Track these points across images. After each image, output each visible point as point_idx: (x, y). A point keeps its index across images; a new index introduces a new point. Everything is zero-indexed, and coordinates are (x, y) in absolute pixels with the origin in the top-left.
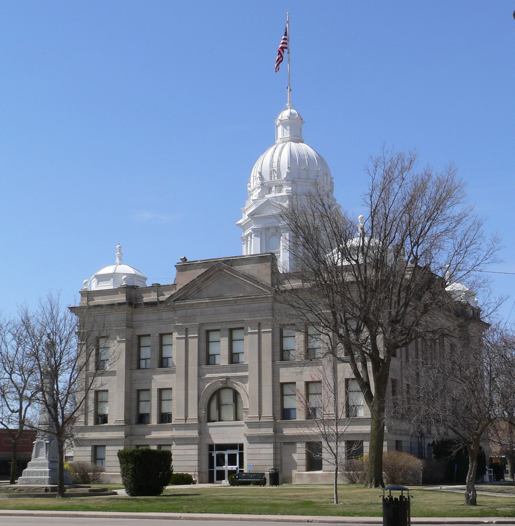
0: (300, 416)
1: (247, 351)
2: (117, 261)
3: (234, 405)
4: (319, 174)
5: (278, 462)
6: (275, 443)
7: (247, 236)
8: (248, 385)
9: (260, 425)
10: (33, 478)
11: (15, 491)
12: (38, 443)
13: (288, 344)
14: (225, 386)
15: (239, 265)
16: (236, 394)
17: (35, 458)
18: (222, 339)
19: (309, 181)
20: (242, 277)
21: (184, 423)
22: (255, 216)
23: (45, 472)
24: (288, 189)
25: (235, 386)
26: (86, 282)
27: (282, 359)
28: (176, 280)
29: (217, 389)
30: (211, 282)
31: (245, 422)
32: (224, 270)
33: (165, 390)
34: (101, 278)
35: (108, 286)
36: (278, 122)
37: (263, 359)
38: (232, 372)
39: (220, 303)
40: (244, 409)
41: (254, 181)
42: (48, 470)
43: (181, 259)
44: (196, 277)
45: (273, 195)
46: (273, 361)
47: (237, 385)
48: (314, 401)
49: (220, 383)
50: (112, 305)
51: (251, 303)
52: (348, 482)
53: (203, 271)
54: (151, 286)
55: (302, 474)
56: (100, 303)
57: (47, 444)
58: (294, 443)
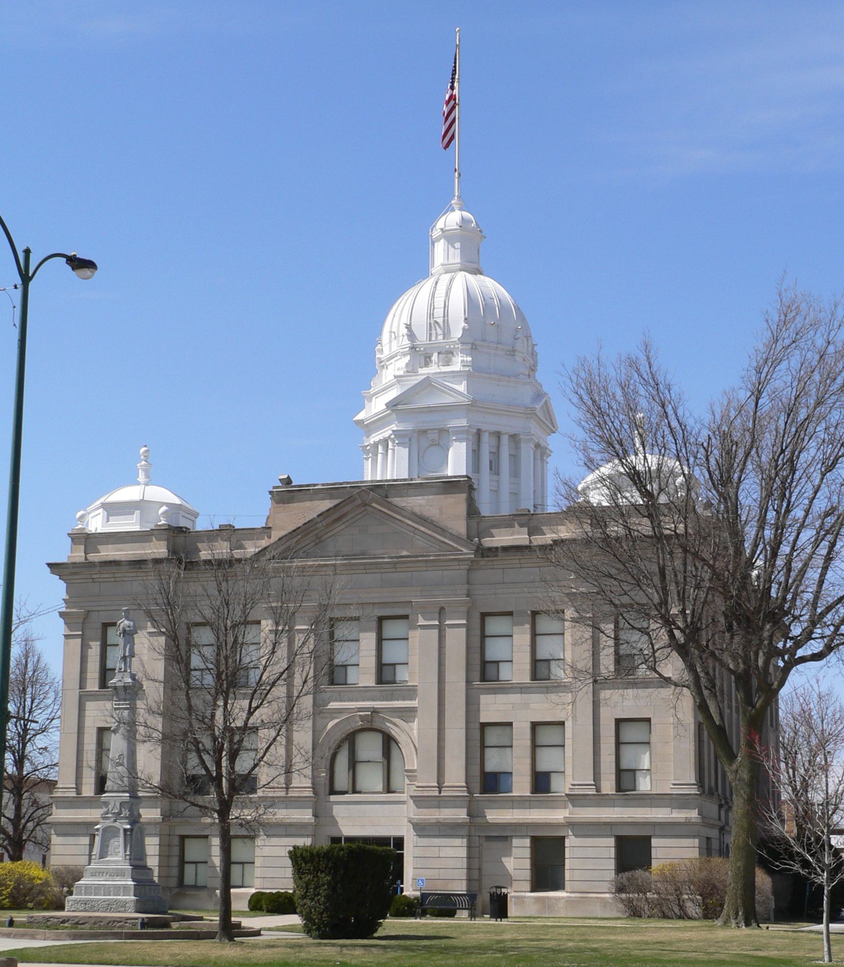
0: (521, 786)
1: (414, 660)
2: (141, 478)
3: (386, 763)
4: (518, 336)
5: (475, 875)
6: (469, 837)
7: (376, 445)
8: (415, 725)
9: (439, 801)
10: (100, 899)
11: (66, 925)
12: (105, 830)
13: (495, 650)
14: (368, 725)
15: (401, 497)
16: (389, 742)
17: (100, 858)
18: (362, 635)
19: (500, 346)
20: (409, 519)
21: (283, 794)
22: (400, 407)
23: (125, 887)
24: (465, 359)
25: (389, 727)
26: (82, 517)
27: (483, 679)
28: (270, 520)
29: (352, 730)
30: (343, 526)
31: (411, 797)
32: (374, 505)
33: (542, 726)
34: (113, 510)
35: (130, 524)
36: (436, 233)
37: (449, 677)
38: (383, 700)
39: (362, 567)
40: (407, 771)
41: (390, 342)
42: (132, 883)
43: (280, 480)
44: (315, 516)
45: (433, 369)
46: (468, 682)
47: (395, 724)
48: (547, 761)
49: (358, 719)
50: (138, 564)
51: (425, 569)
52: (627, 914)
53: (327, 505)
54: (218, 528)
55: (525, 897)
56: (118, 558)
57: (125, 830)
58: (506, 839)
